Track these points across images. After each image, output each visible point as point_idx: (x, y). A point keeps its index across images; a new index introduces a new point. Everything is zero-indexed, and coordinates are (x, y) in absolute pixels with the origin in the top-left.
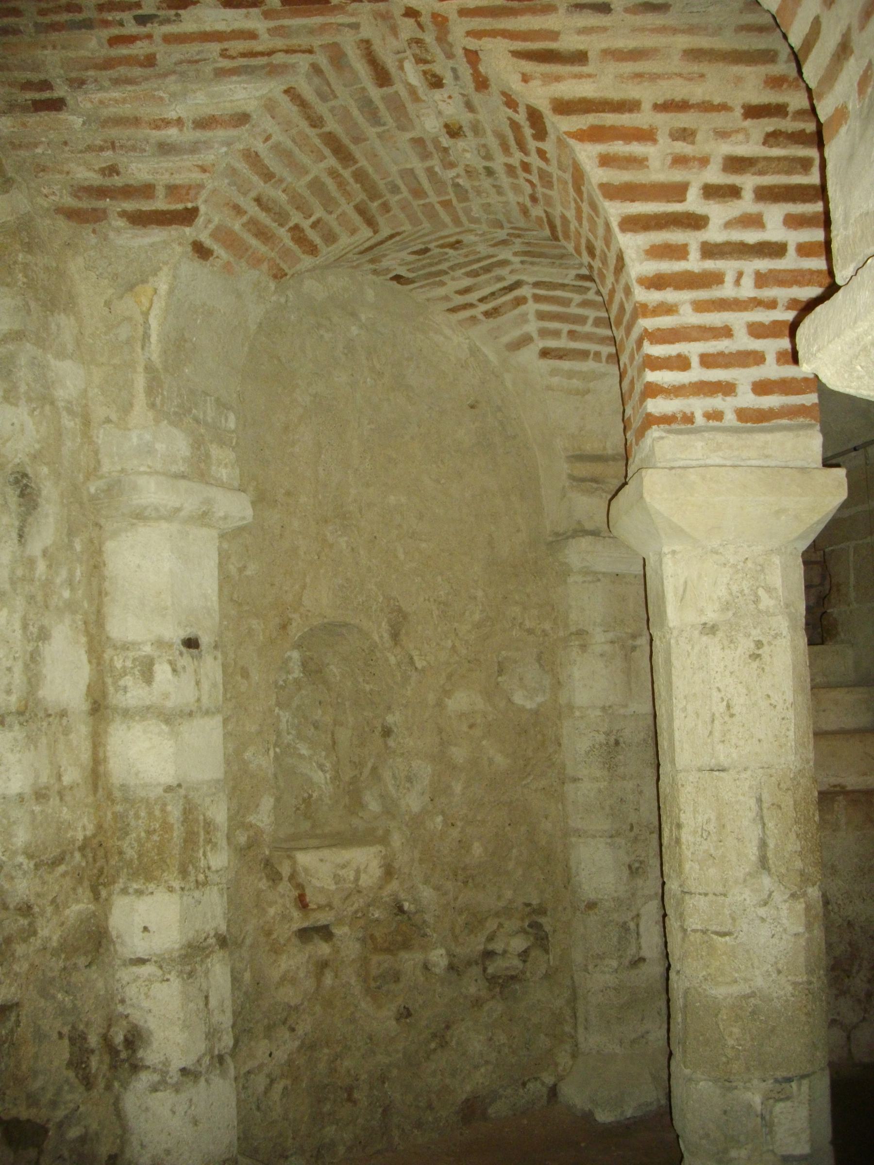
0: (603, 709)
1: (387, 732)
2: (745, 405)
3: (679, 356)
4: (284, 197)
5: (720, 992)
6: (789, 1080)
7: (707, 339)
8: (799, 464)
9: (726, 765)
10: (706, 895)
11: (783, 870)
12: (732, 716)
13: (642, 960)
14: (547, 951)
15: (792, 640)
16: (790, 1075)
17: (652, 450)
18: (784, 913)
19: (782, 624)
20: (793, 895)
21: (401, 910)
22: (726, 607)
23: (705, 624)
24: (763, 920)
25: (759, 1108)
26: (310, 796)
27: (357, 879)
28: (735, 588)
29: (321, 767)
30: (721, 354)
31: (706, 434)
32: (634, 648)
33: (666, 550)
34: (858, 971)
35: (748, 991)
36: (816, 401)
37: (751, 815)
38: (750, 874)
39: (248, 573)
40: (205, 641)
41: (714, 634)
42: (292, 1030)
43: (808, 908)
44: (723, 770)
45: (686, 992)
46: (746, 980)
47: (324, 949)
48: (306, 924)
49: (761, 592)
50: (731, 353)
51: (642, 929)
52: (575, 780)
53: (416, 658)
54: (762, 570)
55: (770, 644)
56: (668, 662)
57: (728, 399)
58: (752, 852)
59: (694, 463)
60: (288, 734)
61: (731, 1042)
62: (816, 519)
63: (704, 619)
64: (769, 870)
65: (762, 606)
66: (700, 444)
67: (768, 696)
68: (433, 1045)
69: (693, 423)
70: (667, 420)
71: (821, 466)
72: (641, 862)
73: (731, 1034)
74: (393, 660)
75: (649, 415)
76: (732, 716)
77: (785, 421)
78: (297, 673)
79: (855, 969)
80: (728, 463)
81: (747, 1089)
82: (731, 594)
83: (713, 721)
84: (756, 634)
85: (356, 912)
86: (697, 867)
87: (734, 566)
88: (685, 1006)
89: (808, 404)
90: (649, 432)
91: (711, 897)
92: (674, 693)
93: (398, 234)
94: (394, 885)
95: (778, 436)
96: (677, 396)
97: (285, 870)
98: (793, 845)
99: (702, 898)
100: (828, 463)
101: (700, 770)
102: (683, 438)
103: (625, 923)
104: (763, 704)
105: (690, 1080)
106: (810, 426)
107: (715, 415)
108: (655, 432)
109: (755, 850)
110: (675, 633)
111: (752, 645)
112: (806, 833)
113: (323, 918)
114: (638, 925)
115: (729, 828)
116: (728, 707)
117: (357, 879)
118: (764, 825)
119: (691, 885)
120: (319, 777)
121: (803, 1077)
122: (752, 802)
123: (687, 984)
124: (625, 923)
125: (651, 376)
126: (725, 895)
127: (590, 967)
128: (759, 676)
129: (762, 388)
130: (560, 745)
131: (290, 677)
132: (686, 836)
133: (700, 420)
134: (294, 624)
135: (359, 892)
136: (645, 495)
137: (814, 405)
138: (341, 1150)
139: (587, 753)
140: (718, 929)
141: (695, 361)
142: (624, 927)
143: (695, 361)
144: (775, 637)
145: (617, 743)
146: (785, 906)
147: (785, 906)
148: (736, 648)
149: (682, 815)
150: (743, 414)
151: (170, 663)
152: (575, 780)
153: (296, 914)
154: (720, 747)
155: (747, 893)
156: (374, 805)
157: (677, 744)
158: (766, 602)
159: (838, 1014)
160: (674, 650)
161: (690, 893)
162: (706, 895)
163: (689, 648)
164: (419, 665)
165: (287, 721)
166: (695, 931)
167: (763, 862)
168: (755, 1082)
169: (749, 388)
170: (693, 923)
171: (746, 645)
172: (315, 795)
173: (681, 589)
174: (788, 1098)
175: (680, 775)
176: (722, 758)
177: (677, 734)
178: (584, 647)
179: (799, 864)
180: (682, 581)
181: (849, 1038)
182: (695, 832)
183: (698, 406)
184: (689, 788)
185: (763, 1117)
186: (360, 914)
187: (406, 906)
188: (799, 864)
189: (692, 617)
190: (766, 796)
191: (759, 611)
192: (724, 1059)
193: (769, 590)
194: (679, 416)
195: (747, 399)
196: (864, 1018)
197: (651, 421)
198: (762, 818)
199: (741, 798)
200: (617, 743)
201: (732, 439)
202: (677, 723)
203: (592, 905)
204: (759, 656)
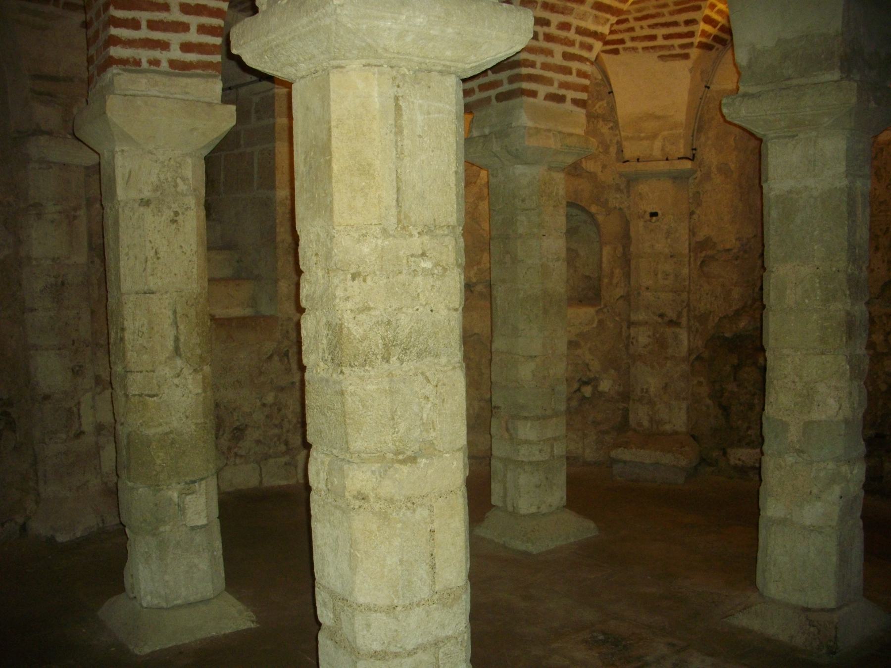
0: (53, 260)
2: (175, 58)
3: (133, 19)
5: (151, 432)
6: (194, 482)
7: (153, 11)
8: (207, 100)
9: (154, 289)
10: (141, 372)
11: (189, 355)
12: (158, 258)
13: (83, 433)
14: (14, 431)
15: (197, 212)
16: (194, 479)
17: (111, 82)
18: (190, 381)
19: (191, 201)
20: (195, 370)
22: (156, 189)
23: (142, 199)
24: (177, 386)
25: (176, 500)
28: (162, 177)
30: (161, 22)
31: (149, 75)
32: (75, 217)
33: (117, 149)
35: (168, 430)
36: (220, 60)
37: (170, 321)
38: (168, 358)
41: (148, 206)
43: (204, 377)
44: (153, 293)
45: (129, 436)
46: (167, 423)
49: (179, 180)
50: (168, 22)
51: (82, 412)
52: (32, 310)
54: (180, 167)
55: (183, 214)
56: (116, 223)
57: (164, 52)
58: (170, 344)
59: (140, 93)
61: (158, 462)
62: (215, 136)
63: (142, 196)
64: (180, 355)
65: (179, 189)
66: (144, 81)
67: (181, 247)
69: (140, 66)
70: (123, 62)
71: (219, 102)
72: (81, 367)
73: (159, 457)
75: (111, 57)
76: (158, 258)
77: (199, 71)
80: (162, 95)
81: (169, 489)
82: (159, 180)
83: (146, 262)
84: (175, 207)
86: (135, 355)
87: (163, 162)
88: (128, 443)
89: (215, 62)
90: (110, 69)
91: (144, 373)
92: (121, 244)
95: (195, 80)
96: (130, 47)
98: (195, 340)
99: (139, 374)
100: (225, 100)
101: (137, 293)
102: (134, 75)
103: (70, 408)
104: (178, 251)
105: (133, 488)
106: (215, 76)
107: (155, 62)
108: (114, 70)
109: (172, 343)
110: (122, 204)
111: (172, 214)
112: (203, 332)
114: (79, 410)
115: (156, 329)
116: (156, 253)
118: (177, 327)
119: (132, 366)
121: (202, 479)
122: (170, 313)
123: (130, 429)
124: (70, 408)
125: (114, 31)
126: (154, 371)
127: (47, 440)
128: (176, 234)
129: (187, 47)
130: (20, 285)
132: (128, 335)
133: (145, 65)
136: (107, 112)
137: (218, 63)
139: (41, 291)
140: (150, 393)
141: (193, 29)
142: (70, 410)
143: (144, 24)
144: (186, 209)
145: (63, 284)
146: (191, 377)
147: (191, 377)
148: (162, 215)
149: (125, 323)
150: (173, 63)
152: (32, 310)
154: (151, 278)
155: (167, 370)
157: (122, 276)
158: (182, 187)
160: (121, 217)
161: (131, 372)
162: (141, 372)
163: (131, 214)
166: (134, 395)
167: (177, 351)
168: (174, 485)
169: (178, 47)
170: (133, 390)
171: (168, 214)
173: (127, 176)
174: (193, 493)
175: (125, 297)
176: (151, 285)
177: (122, 271)
178: (39, 216)
179: (199, 351)
180: (128, 170)
182: (134, 333)
183: (144, 55)
184: (130, 305)
185: (179, 506)
188: (199, 351)
189: (133, 194)
190: (179, 310)
191: (177, 192)
192: (154, 473)
193: (184, 179)
194: (131, 60)
195: (176, 53)
197: (111, 61)
198: (176, 323)
199: (164, 310)
200: (63, 284)
201: (165, 80)
202: (122, 263)
203: (46, 397)
204: (176, 221)
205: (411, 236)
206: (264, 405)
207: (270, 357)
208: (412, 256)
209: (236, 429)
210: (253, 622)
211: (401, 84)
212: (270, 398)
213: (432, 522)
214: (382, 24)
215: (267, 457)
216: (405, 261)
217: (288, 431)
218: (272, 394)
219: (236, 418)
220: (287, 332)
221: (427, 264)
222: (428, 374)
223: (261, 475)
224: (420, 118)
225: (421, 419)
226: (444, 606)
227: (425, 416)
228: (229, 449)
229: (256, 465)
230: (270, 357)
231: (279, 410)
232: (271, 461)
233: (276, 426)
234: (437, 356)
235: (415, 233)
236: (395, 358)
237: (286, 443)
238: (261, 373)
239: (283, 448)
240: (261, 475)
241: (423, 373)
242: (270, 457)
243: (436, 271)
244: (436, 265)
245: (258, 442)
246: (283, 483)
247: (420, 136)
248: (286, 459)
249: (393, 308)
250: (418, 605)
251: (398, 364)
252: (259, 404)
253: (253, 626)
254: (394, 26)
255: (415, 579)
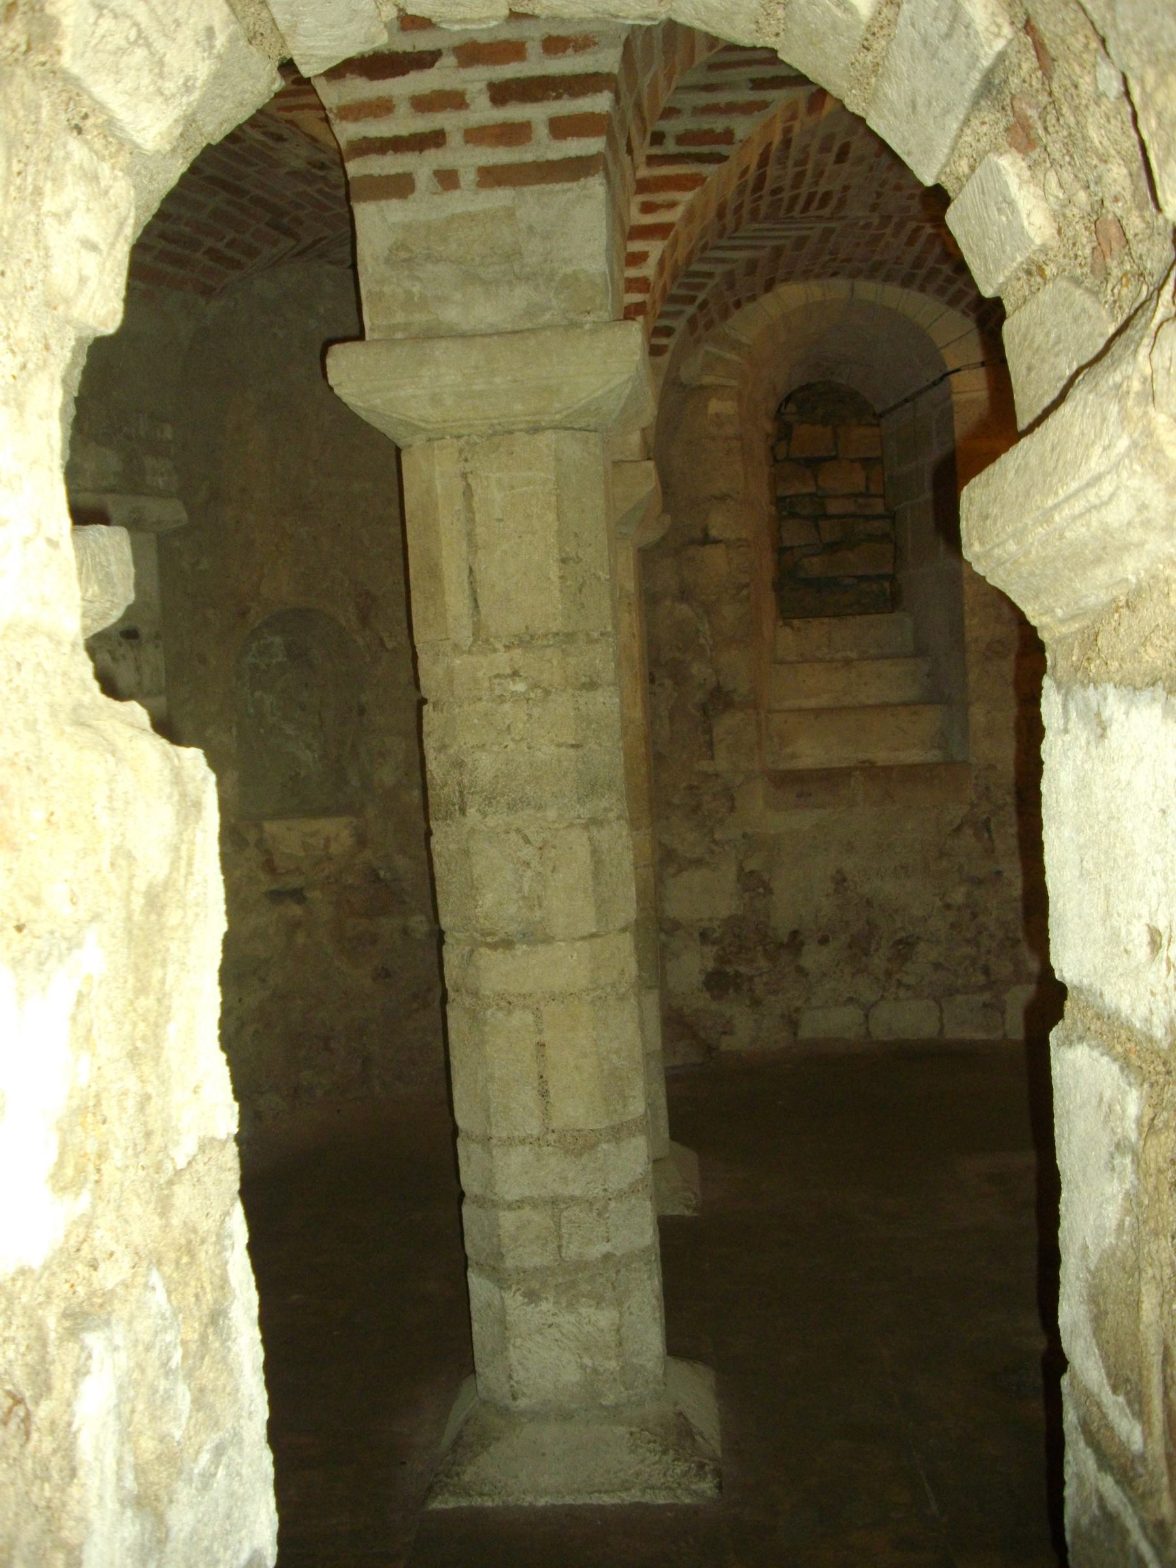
1: (362, 711)
4: (187, 230)
21: (377, 879)
26: (298, 774)
27: (327, 847)
29: (309, 747)
34: (877, 950)
39: (201, 567)
40: (144, 631)
42: (263, 980)
47: (296, 910)
48: (274, 887)
53: (385, 639)
60: (273, 715)
68: (415, 1006)
74: (361, 642)
78: (281, 658)
79: (873, 947)
85: (328, 877)
93: (321, 240)
94: (368, 854)
97: (252, 837)
113: (295, 882)
117: (327, 847)
120: (307, 756)
131: (274, 661)
134: (252, 612)
135: (330, 859)
138: (319, 1093)
151: (109, 652)
153: (262, 876)
156: (355, 781)
159: (855, 992)
164: (390, 645)
165: (272, 704)
172: (303, 773)
181: (867, 1016)
186: (332, 880)
187: (382, 873)
196: (882, 996)
205: (495, 650)
206: (948, 907)
207: (958, 829)
208: (497, 676)
209: (900, 941)
210: (688, 1207)
211: (469, 457)
212: (958, 896)
213: (540, 1032)
214: (402, 393)
215: (951, 992)
216: (486, 684)
217: (989, 952)
218: (963, 889)
219: (899, 924)
220: (987, 788)
221: (520, 687)
222: (526, 832)
223: (941, 1019)
224: (498, 496)
225: (520, 891)
226: (566, 1152)
227: (526, 888)
228: (889, 974)
229: (932, 1003)
230: (958, 829)
231: (974, 916)
232: (960, 998)
233: (968, 941)
234: (539, 808)
235: (499, 646)
236: (473, 810)
237: (986, 971)
238: (942, 854)
239: (981, 979)
240: (941, 1019)
241: (518, 831)
242: (957, 991)
243: (532, 695)
244: (535, 686)
245: (937, 966)
246: (980, 1036)
247: (500, 520)
248: (986, 996)
249: (469, 745)
250: (523, 1142)
251: (479, 817)
252: (939, 904)
253: (687, 1213)
254: (418, 392)
255: (514, 1105)
